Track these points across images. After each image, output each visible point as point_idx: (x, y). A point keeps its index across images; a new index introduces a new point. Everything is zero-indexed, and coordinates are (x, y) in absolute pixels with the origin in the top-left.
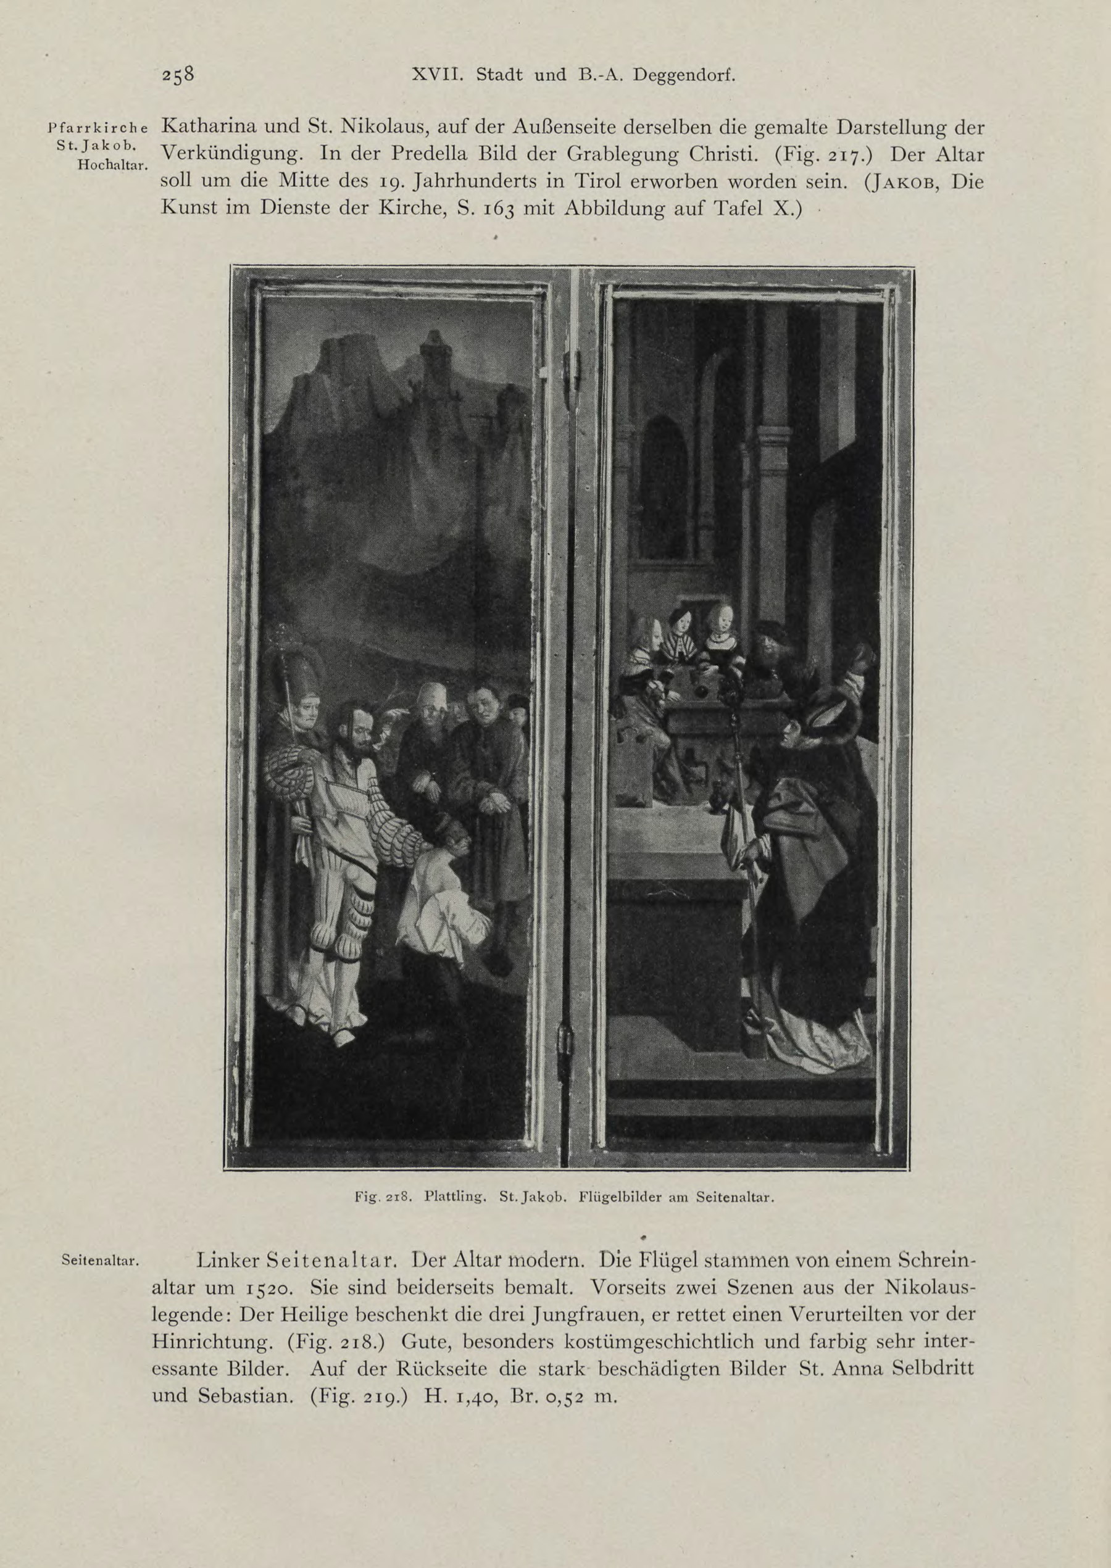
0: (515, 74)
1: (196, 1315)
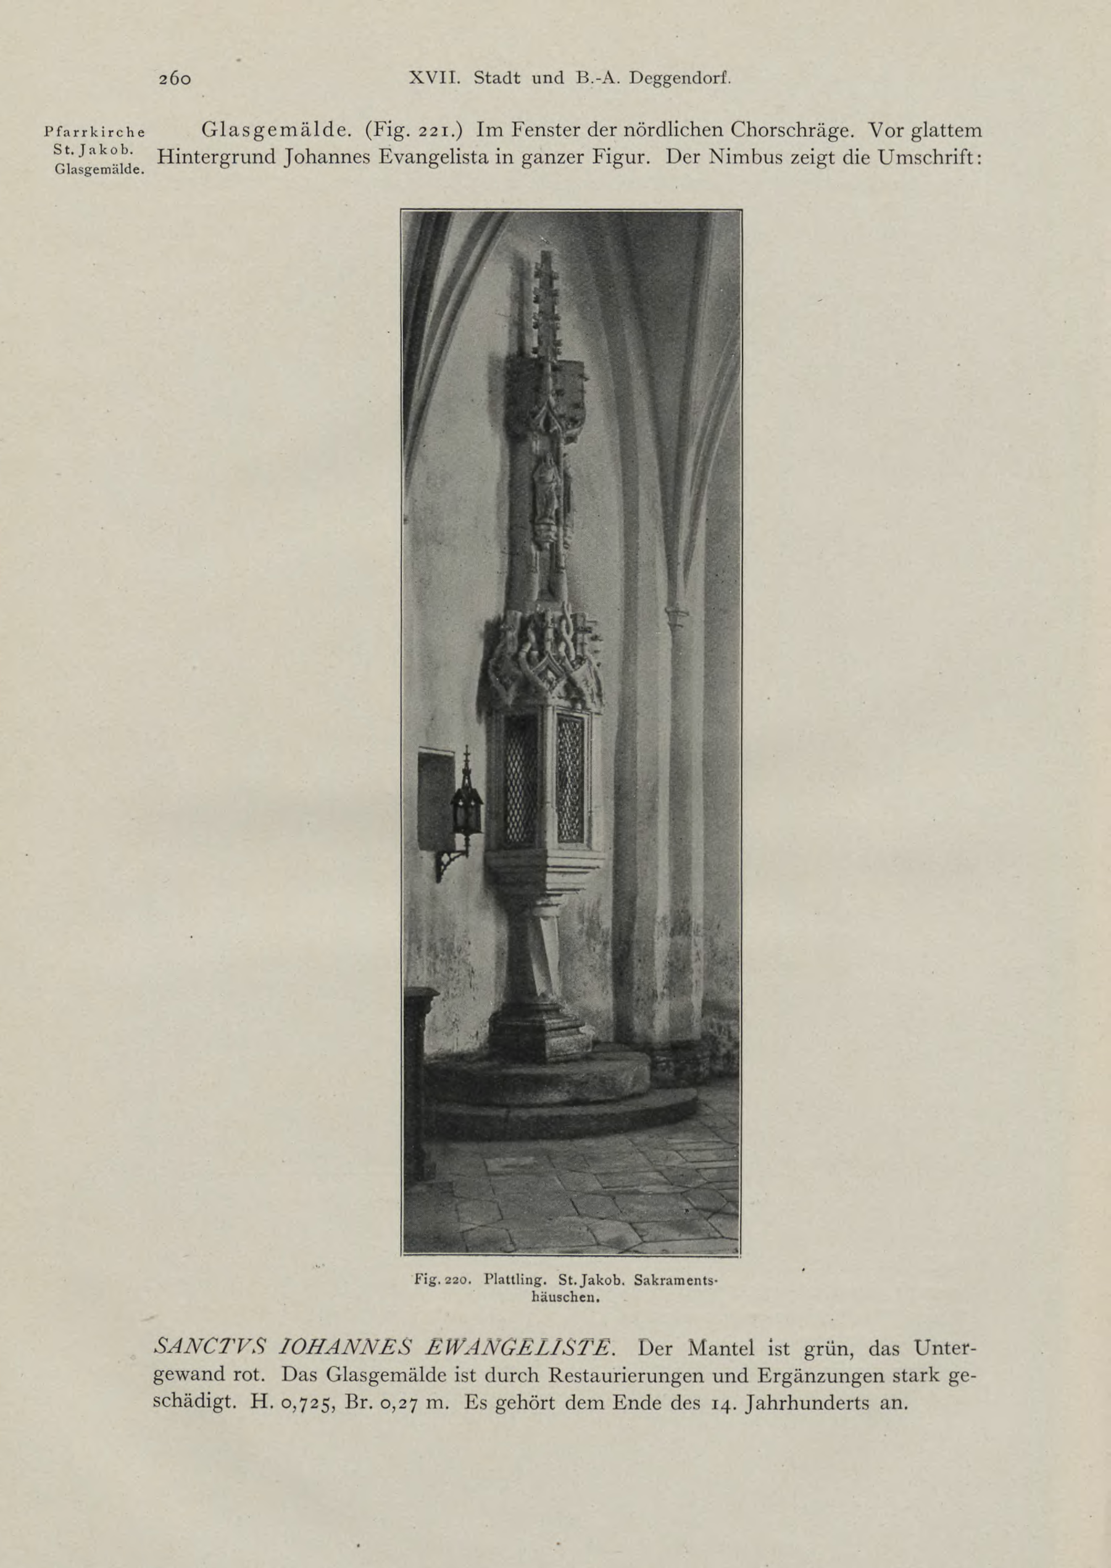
0: (514, 78)
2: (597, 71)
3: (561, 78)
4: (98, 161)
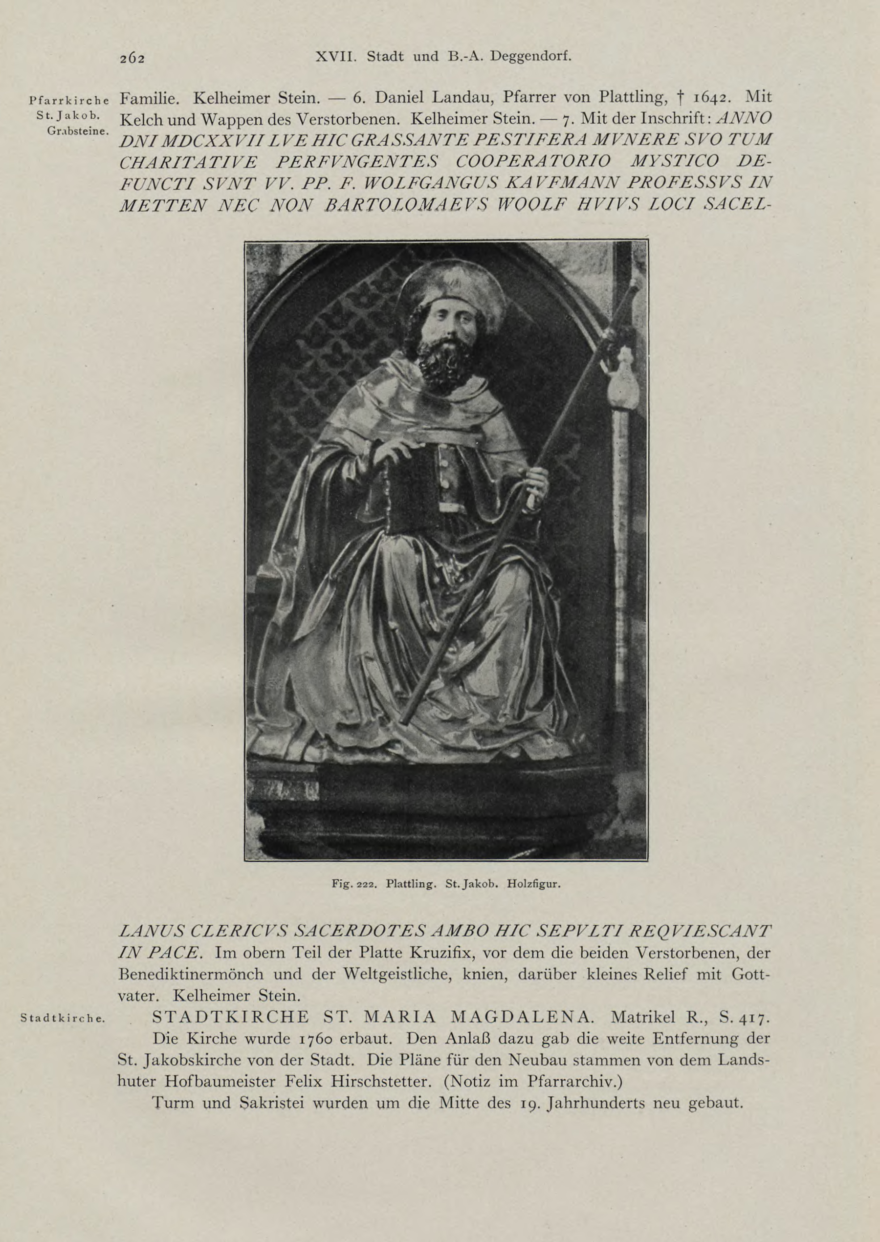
0: (398, 56)
1: (143, 975)
2: (464, 51)
3: (436, 57)
4: (75, 124)
